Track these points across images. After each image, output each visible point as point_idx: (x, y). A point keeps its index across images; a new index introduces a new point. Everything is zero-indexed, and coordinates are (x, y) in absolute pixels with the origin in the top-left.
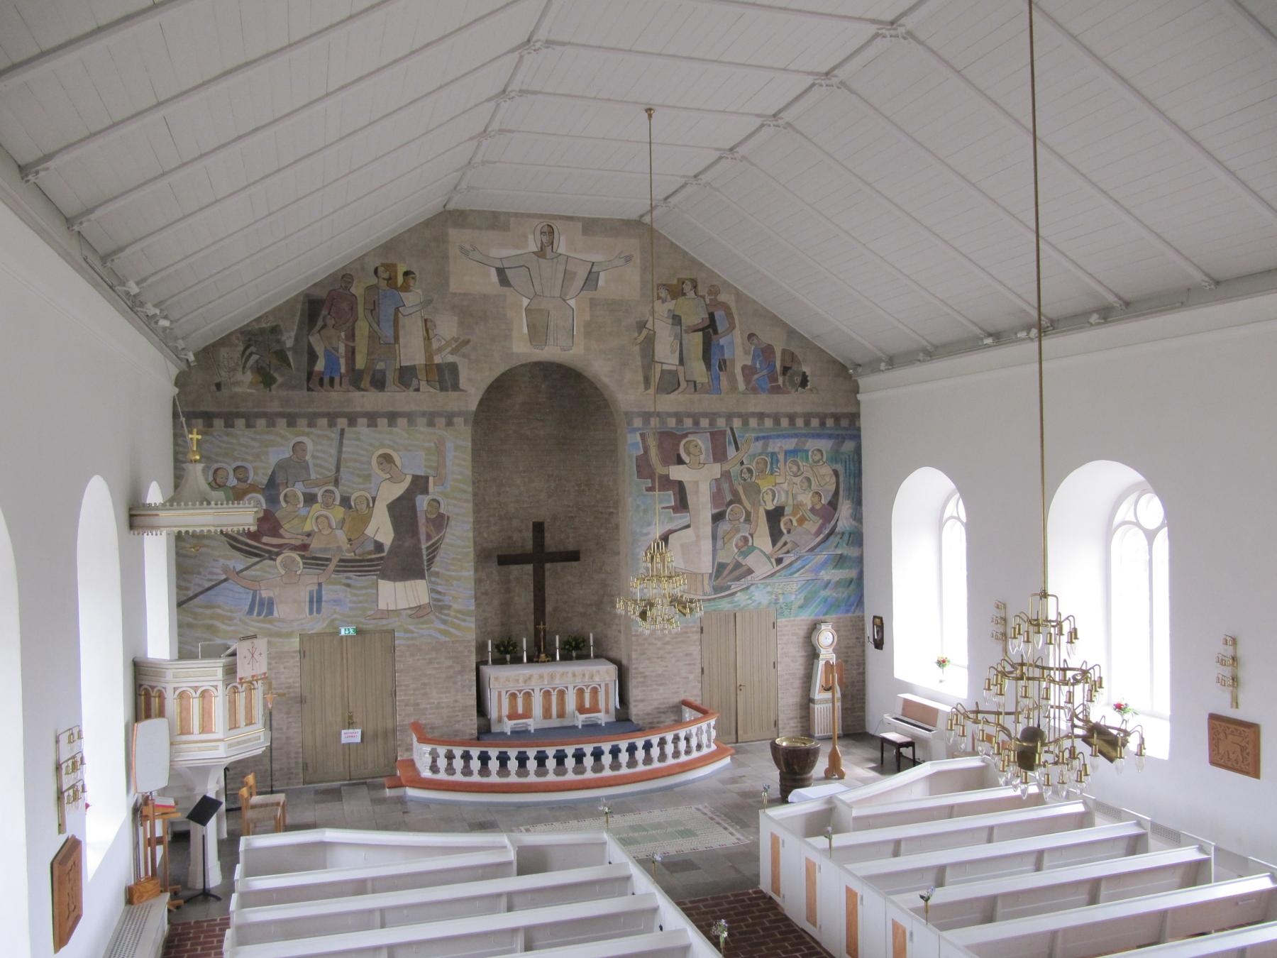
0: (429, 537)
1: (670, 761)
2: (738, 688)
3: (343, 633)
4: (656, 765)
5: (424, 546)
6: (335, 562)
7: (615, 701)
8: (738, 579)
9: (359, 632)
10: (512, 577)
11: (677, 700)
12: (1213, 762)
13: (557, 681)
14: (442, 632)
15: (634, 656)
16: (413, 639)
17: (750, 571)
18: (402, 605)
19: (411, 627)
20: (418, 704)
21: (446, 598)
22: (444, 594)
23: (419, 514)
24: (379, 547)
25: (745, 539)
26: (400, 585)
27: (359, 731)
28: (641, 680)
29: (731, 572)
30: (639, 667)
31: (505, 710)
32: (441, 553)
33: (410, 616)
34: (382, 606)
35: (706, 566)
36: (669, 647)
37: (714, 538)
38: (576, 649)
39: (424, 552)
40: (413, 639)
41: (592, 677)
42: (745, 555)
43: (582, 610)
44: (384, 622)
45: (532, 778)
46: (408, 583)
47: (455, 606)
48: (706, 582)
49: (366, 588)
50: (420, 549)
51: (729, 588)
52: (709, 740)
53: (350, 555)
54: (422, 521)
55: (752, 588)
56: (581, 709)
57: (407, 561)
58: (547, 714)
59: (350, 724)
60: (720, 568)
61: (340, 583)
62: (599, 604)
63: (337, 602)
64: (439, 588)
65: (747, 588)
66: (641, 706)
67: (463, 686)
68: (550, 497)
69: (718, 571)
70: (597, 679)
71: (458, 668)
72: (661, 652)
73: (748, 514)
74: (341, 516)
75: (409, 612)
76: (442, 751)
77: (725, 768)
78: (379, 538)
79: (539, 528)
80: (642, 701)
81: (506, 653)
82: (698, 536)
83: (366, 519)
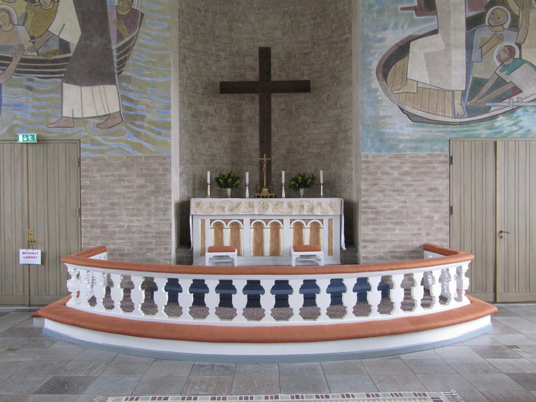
0: (120, 37)
1: (398, 313)
2: (498, 235)
3: (21, 139)
4: (375, 316)
5: (114, 47)
6: (16, 61)
7: (339, 241)
8: (500, 99)
9: (41, 141)
10: (244, 117)
11: (417, 243)
12: (216, 314)
13: (270, 212)
14: (134, 146)
15: (363, 187)
16: (102, 152)
17: (516, 90)
18: (89, 112)
19: (99, 139)
20: (106, 227)
21: (139, 107)
22: (137, 103)
23: (109, 10)
24: (64, 46)
25: (511, 50)
26: (87, 90)
27: (39, 251)
28: (373, 216)
29: (488, 93)
30: (372, 201)
31: (210, 242)
32: (134, 55)
33: (98, 126)
34: (67, 112)
35: (457, 80)
36: (408, 178)
37: (469, 47)
38: (303, 185)
39: (115, 53)
40: (102, 152)
41: (312, 209)
42: (511, 69)
43: (315, 151)
44: (68, 131)
45: (240, 321)
46: (96, 88)
47: (149, 116)
48: (457, 101)
49: (48, 92)
50: (111, 50)
51: (487, 110)
52: (459, 291)
53: (33, 55)
54: (112, 17)
55: (519, 111)
56: (298, 246)
57: (96, 65)
58: (259, 250)
59: (31, 244)
60: (476, 86)
61: (21, 86)
62: (334, 143)
63: (19, 106)
64: (132, 96)
65: (513, 111)
66: (371, 247)
67: (157, 210)
68: (284, 34)
69: (472, 89)
70: (318, 212)
71: (151, 187)
72: (398, 184)
73: (515, 19)
74: (24, 10)
75: (97, 121)
76: (117, 277)
77: (483, 333)
78: (65, 36)
79: (265, 54)
80: (372, 241)
81: (228, 184)
82: (447, 45)
83: (50, 15)
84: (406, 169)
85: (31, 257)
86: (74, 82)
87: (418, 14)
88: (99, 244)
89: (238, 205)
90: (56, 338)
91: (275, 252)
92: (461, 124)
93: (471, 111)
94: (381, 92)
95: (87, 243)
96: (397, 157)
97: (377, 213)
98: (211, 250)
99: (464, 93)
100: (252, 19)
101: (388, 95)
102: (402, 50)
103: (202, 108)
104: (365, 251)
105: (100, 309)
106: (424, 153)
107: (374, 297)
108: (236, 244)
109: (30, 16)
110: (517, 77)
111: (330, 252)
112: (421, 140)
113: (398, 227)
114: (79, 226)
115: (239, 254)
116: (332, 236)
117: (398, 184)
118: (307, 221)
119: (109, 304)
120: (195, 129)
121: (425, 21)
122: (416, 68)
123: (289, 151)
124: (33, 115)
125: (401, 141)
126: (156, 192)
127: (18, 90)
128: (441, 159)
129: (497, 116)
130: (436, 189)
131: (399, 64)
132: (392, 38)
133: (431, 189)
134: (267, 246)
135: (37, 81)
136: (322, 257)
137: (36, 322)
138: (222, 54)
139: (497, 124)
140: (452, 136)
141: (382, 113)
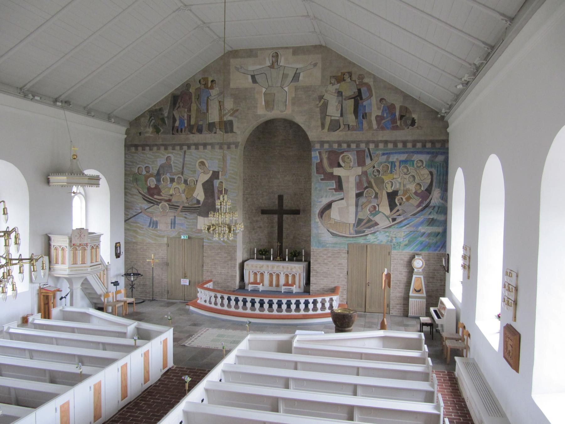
7: (303, 282)
8: (369, 227)
9: (189, 238)
17: (376, 224)
23: (215, 188)
24: (198, 202)
25: (374, 207)
27: (188, 280)
35: (352, 219)
37: (357, 205)
41: (291, 269)
42: (375, 215)
43: (305, 239)
44: (199, 235)
48: (351, 228)
49: (192, 219)
53: (187, 205)
58: (271, 284)
59: (185, 277)
60: (359, 222)
63: (182, 224)
67: (231, 266)
70: (294, 270)
71: (229, 258)
72: (326, 261)
78: (199, 198)
79: (281, 198)
80: (315, 284)
81: (263, 254)
82: (348, 204)
83: (193, 190)
84: (329, 255)
85: (185, 282)
86: (202, 216)
87: (336, 192)
88: (210, 278)
89: (263, 266)
90: (193, 312)
91: (278, 285)
92: (353, 237)
93: (357, 232)
94: (320, 224)
95: (206, 277)
96: (325, 250)
97: (317, 272)
98: (252, 283)
99: (354, 225)
100: (279, 177)
101: (322, 224)
102: (329, 206)
103: (254, 219)
104: (313, 287)
105: (207, 304)
106: (337, 249)
107: (311, 306)
108: (262, 281)
109: (186, 190)
110: (377, 219)
111: (299, 287)
112: (336, 244)
113: (325, 279)
114: (203, 271)
115: (263, 285)
116: (301, 280)
117: (326, 261)
118: (290, 274)
119: (216, 304)
120: (251, 228)
121: (339, 194)
122: (334, 213)
123: (294, 237)
124: (187, 228)
125: (327, 243)
126: (231, 260)
127: (181, 218)
128: (344, 251)
129: (368, 235)
130: (342, 264)
131: (327, 212)
132: (325, 201)
133: (339, 264)
134: (274, 283)
135: (189, 215)
136: (295, 289)
137: (187, 307)
138: (265, 194)
139: (368, 238)
140: (349, 242)
141: (320, 232)
